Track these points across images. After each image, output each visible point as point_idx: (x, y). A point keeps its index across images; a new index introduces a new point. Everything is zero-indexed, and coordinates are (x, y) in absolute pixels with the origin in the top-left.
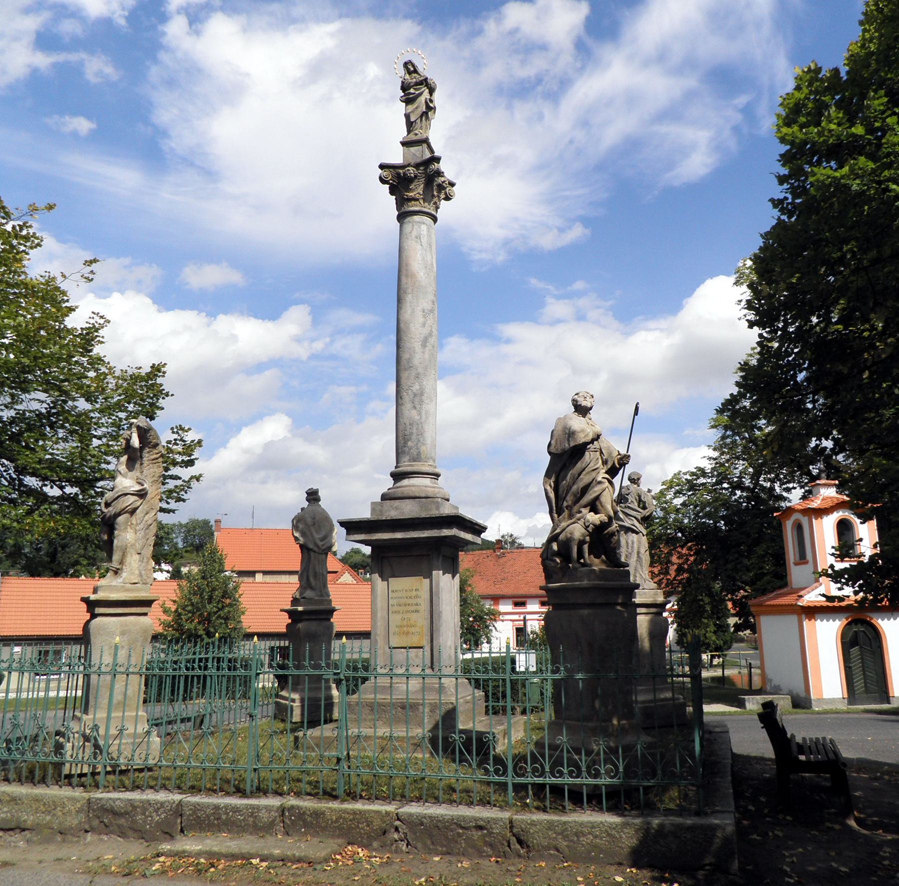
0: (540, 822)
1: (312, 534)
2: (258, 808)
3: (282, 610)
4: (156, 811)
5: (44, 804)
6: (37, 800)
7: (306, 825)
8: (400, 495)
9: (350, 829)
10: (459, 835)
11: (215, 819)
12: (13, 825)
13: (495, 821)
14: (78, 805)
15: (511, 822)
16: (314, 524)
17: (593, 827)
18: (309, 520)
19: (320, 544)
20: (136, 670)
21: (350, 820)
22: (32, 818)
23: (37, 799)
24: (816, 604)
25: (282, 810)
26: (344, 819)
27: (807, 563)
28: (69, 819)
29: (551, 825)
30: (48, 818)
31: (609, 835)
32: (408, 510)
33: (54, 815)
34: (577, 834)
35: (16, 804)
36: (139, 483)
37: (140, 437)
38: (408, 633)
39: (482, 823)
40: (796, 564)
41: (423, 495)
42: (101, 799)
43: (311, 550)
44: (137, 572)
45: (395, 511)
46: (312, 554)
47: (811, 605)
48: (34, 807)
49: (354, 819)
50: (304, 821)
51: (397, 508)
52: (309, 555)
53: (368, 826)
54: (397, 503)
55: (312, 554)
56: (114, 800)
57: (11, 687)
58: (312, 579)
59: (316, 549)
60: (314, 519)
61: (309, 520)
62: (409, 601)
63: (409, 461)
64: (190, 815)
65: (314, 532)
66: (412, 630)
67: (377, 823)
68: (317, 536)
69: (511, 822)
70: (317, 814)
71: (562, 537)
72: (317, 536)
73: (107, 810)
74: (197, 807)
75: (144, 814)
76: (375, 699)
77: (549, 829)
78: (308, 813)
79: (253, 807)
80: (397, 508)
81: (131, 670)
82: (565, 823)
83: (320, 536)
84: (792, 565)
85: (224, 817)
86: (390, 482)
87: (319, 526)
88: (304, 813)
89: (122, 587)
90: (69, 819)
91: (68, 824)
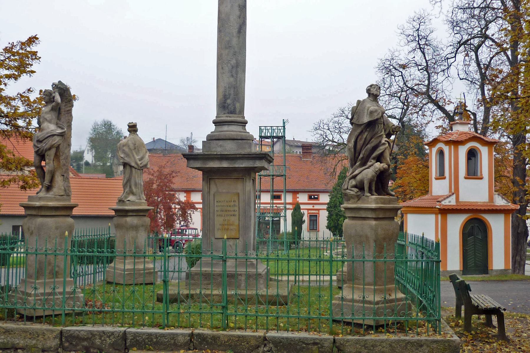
0: (352, 340)
1: (133, 156)
2: (177, 334)
3: (110, 208)
4: (109, 337)
5: (30, 334)
6: (24, 331)
7: (208, 343)
8: (223, 137)
9: (236, 345)
10: (304, 348)
11: (149, 341)
12: (9, 346)
13: (326, 340)
14: (55, 334)
15: (334, 339)
16: (135, 149)
17: (382, 342)
18: (132, 146)
19: (139, 163)
20: (62, 252)
21: (236, 341)
22: (22, 342)
23: (25, 331)
24: (449, 207)
25: (192, 335)
26: (233, 340)
27: (445, 178)
28: (48, 342)
29: (357, 342)
30: (34, 342)
31: (391, 345)
32: (230, 148)
33: (38, 340)
34: (372, 346)
35: (10, 334)
36: (60, 127)
37: (61, 95)
38: (228, 229)
39: (318, 341)
40: (436, 179)
41: (239, 138)
42: (70, 331)
43: (133, 167)
44: (63, 188)
45: (219, 148)
46: (133, 170)
47: (446, 208)
48: (23, 335)
49: (238, 340)
50: (207, 341)
51: (221, 146)
52: (131, 171)
53: (248, 344)
54: (221, 143)
55: (133, 170)
56: (79, 331)
57: (333, 270)
58: (133, 188)
59: (136, 166)
60: (135, 144)
61: (132, 146)
62: (229, 208)
63: (228, 113)
64: (132, 339)
65: (135, 154)
66: (231, 227)
67: (253, 343)
68: (137, 157)
69: (334, 339)
70: (215, 338)
71: (359, 178)
72: (137, 157)
73: (74, 337)
74: (135, 335)
75: (100, 339)
76: (236, 271)
77: (357, 343)
78: (209, 337)
79: (173, 334)
80: (221, 146)
81: (147, 254)
82: (366, 340)
83: (139, 157)
84: (433, 179)
85: (155, 340)
86: (213, 128)
87: (138, 150)
88: (207, 337)
89: (55, 197)
90: (48, 342)
91: (48, 345)
